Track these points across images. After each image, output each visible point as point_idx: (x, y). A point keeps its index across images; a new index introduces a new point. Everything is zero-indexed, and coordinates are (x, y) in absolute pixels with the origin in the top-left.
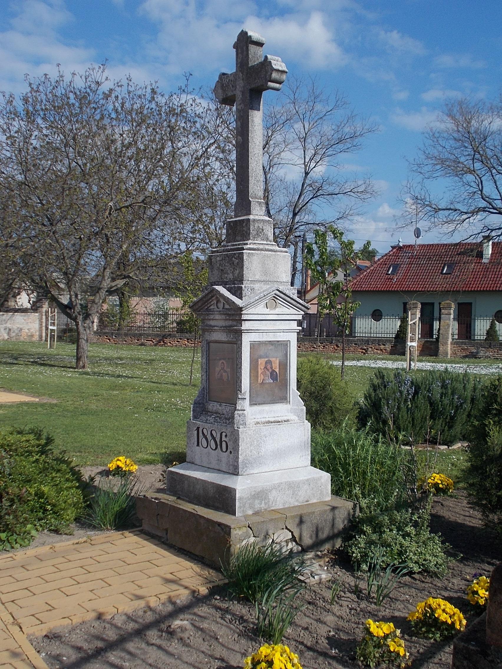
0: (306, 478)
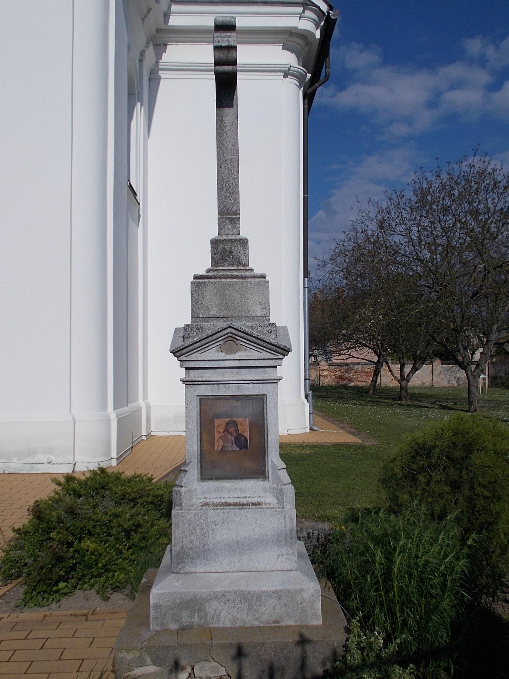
0: (274, 589)
